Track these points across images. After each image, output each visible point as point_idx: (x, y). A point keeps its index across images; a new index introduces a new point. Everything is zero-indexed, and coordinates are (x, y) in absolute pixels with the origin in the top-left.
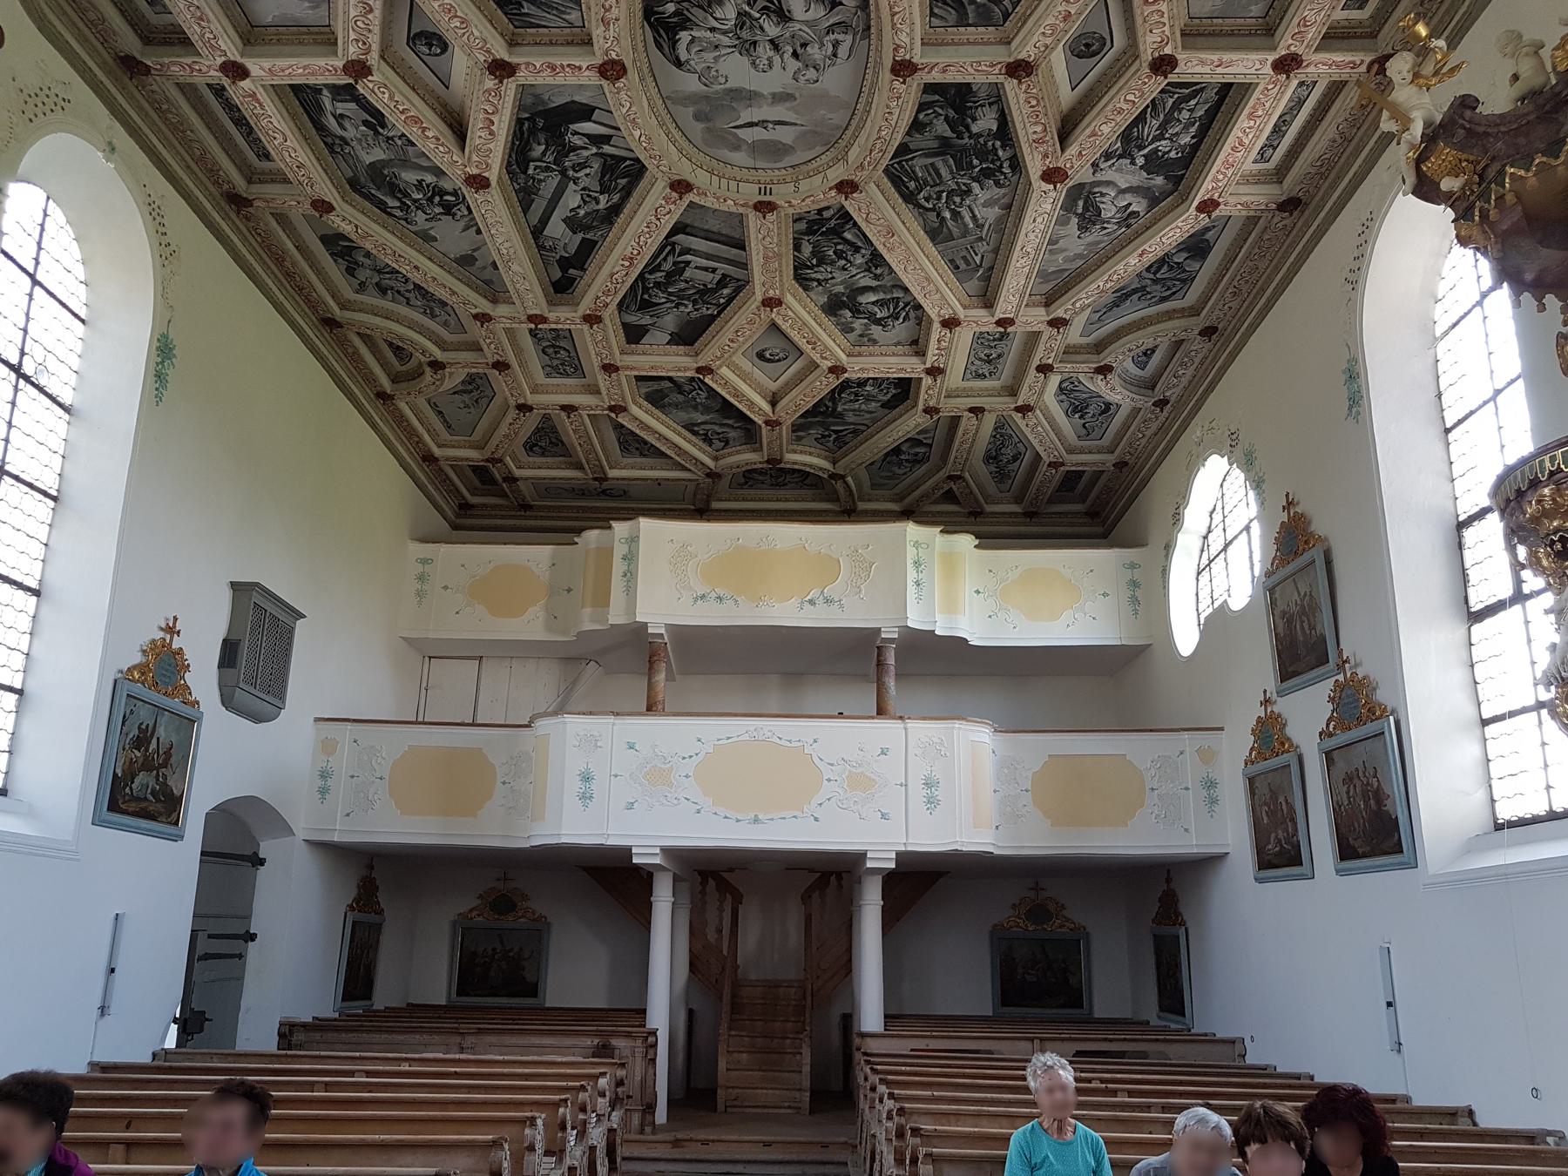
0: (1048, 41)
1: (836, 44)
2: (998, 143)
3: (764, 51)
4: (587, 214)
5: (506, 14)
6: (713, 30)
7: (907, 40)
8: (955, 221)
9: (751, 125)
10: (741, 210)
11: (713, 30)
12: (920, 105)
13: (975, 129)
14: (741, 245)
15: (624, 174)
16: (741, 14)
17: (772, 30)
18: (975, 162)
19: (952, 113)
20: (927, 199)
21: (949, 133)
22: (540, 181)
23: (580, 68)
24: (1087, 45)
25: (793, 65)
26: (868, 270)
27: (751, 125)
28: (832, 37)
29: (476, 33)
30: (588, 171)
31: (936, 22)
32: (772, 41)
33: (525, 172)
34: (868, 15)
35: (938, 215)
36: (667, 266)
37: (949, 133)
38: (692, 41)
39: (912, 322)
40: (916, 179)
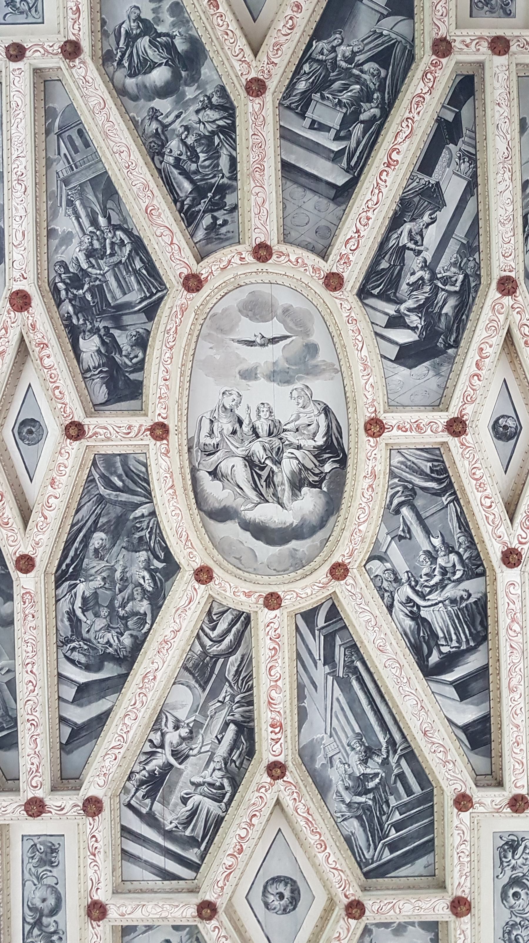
0: (61, 459)
1: (211, 433)
2: (75, 321)
3: (263, 427)
4: (421, 215)
5: (443, 462)
6: (299, 447)
7: (161, 461)
8: (93, 211)
9: (274, 341)
10: (283, 248)
11: (299, 447)
12: (142, 369)
13: (96, 339)
14: (288, 168)
15: (380, 282)
16: (278, 462)
17: (257, 449)
18: (89, 297)
19: (117, 357)
20: (122, 244)
21: (116, 333)
22: (454, 264)
23: (399, 428)
24: (30, 432)
25: (241, 412)
26: (165, 127)
27: (274, 341)
28: (215, 441)
29: (466, 462)
30: (413, 279)
31: (142, 458)
32: (258, 437)
33: (466, 276)
34: (190, 462)
35: (109, 219)
36: (357, 130)
37: (116, 333)
38: (315, 434)
39: (110, 28)
40: (136, 273)
